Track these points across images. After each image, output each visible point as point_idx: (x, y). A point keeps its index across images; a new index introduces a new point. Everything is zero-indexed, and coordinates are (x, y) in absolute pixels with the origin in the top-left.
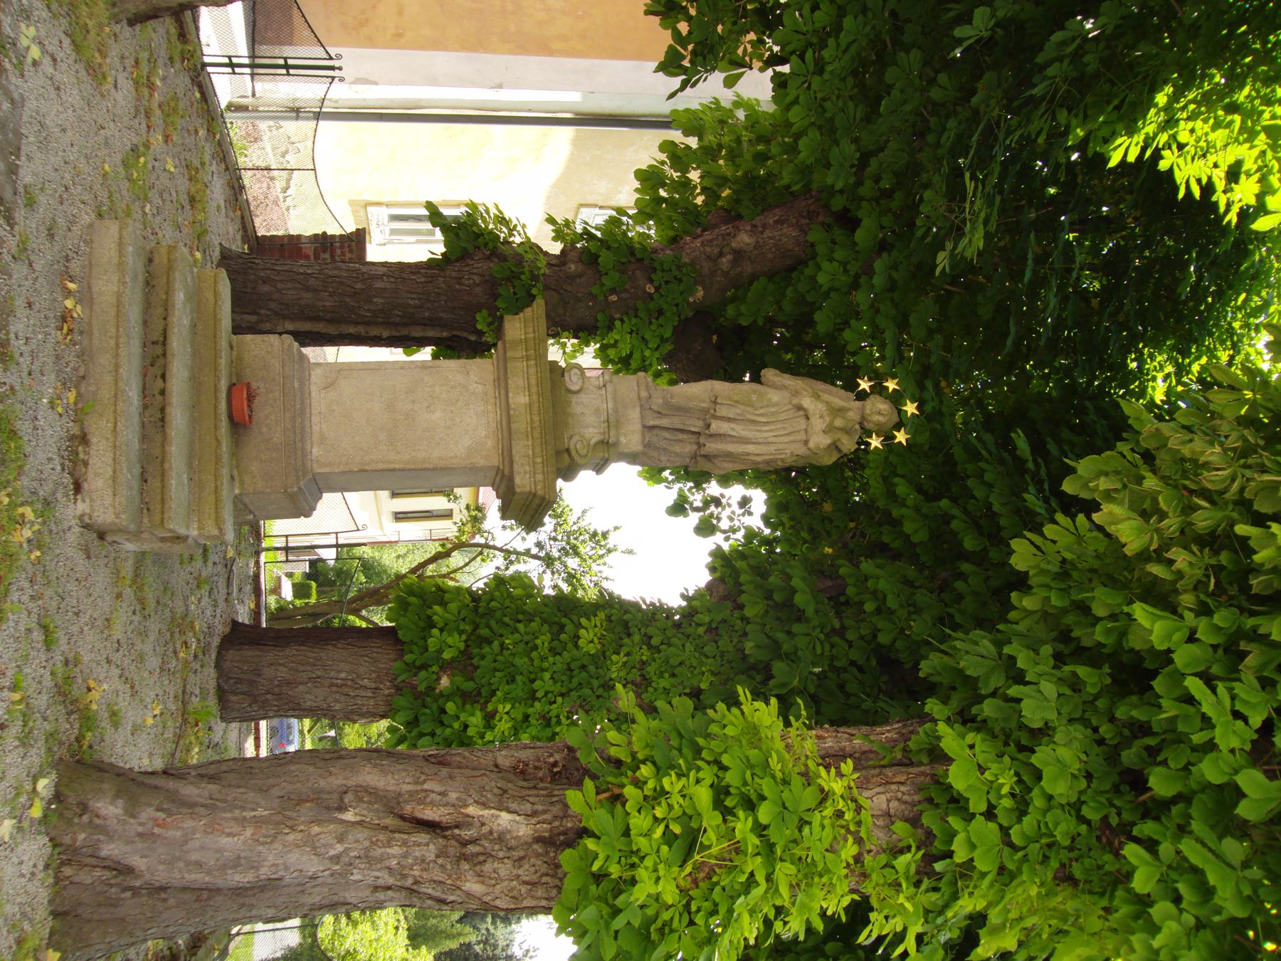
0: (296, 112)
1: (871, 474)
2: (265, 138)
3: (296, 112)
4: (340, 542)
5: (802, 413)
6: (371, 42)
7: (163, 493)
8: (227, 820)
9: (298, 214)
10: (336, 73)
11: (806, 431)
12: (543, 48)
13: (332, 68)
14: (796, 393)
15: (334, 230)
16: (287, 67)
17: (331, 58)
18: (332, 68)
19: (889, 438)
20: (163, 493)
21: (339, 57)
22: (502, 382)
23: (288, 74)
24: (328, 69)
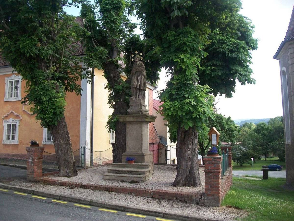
0: (92, 156)
1: (40, 169)
2: (96, 162)
3: (92, 156)
4: (169, 160)
5: (136, 72)
6: (79, 141)
7: (5, 72)
8: (261, 212)
9: (109, 155)
10: (84, 147)
11: (139, 72)
12: (79, 109)
13: (83, 147)
14: (133, 73)
15: (112, 149)
16: (83, 155)
17: (82, 147)
18: (83, 147)
19: (141, 56)
20: (5, 72)
21: (81, 146)
22: (130, 123)
23: (84, 155)
24: (84, 148)
